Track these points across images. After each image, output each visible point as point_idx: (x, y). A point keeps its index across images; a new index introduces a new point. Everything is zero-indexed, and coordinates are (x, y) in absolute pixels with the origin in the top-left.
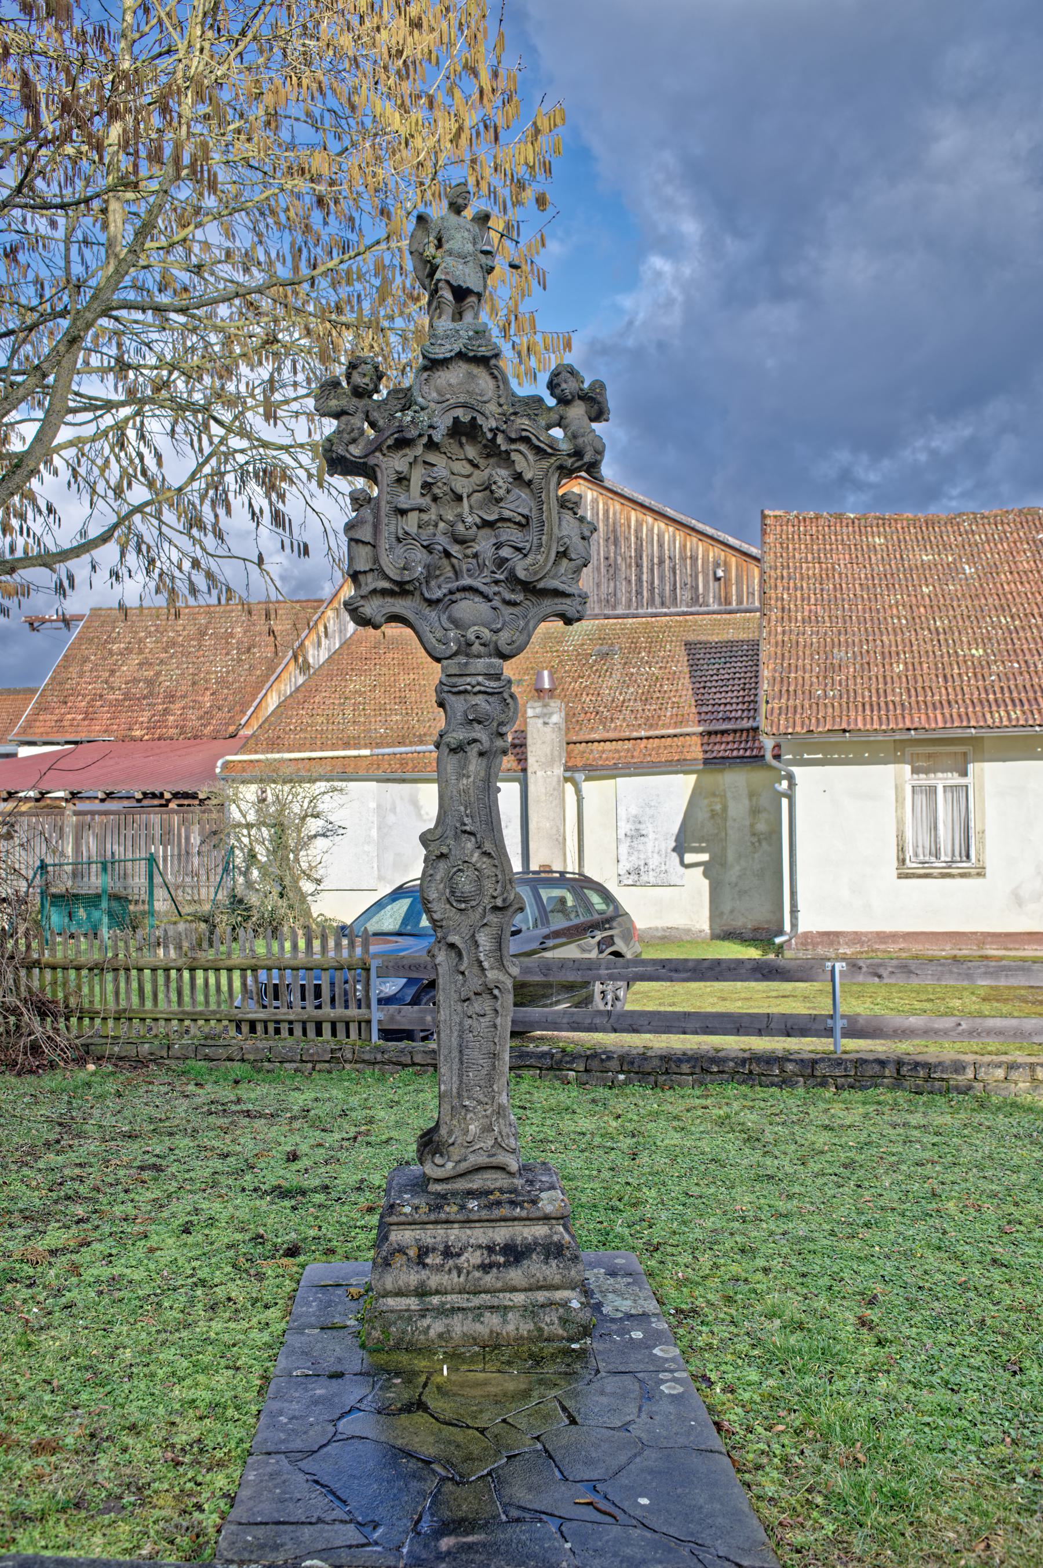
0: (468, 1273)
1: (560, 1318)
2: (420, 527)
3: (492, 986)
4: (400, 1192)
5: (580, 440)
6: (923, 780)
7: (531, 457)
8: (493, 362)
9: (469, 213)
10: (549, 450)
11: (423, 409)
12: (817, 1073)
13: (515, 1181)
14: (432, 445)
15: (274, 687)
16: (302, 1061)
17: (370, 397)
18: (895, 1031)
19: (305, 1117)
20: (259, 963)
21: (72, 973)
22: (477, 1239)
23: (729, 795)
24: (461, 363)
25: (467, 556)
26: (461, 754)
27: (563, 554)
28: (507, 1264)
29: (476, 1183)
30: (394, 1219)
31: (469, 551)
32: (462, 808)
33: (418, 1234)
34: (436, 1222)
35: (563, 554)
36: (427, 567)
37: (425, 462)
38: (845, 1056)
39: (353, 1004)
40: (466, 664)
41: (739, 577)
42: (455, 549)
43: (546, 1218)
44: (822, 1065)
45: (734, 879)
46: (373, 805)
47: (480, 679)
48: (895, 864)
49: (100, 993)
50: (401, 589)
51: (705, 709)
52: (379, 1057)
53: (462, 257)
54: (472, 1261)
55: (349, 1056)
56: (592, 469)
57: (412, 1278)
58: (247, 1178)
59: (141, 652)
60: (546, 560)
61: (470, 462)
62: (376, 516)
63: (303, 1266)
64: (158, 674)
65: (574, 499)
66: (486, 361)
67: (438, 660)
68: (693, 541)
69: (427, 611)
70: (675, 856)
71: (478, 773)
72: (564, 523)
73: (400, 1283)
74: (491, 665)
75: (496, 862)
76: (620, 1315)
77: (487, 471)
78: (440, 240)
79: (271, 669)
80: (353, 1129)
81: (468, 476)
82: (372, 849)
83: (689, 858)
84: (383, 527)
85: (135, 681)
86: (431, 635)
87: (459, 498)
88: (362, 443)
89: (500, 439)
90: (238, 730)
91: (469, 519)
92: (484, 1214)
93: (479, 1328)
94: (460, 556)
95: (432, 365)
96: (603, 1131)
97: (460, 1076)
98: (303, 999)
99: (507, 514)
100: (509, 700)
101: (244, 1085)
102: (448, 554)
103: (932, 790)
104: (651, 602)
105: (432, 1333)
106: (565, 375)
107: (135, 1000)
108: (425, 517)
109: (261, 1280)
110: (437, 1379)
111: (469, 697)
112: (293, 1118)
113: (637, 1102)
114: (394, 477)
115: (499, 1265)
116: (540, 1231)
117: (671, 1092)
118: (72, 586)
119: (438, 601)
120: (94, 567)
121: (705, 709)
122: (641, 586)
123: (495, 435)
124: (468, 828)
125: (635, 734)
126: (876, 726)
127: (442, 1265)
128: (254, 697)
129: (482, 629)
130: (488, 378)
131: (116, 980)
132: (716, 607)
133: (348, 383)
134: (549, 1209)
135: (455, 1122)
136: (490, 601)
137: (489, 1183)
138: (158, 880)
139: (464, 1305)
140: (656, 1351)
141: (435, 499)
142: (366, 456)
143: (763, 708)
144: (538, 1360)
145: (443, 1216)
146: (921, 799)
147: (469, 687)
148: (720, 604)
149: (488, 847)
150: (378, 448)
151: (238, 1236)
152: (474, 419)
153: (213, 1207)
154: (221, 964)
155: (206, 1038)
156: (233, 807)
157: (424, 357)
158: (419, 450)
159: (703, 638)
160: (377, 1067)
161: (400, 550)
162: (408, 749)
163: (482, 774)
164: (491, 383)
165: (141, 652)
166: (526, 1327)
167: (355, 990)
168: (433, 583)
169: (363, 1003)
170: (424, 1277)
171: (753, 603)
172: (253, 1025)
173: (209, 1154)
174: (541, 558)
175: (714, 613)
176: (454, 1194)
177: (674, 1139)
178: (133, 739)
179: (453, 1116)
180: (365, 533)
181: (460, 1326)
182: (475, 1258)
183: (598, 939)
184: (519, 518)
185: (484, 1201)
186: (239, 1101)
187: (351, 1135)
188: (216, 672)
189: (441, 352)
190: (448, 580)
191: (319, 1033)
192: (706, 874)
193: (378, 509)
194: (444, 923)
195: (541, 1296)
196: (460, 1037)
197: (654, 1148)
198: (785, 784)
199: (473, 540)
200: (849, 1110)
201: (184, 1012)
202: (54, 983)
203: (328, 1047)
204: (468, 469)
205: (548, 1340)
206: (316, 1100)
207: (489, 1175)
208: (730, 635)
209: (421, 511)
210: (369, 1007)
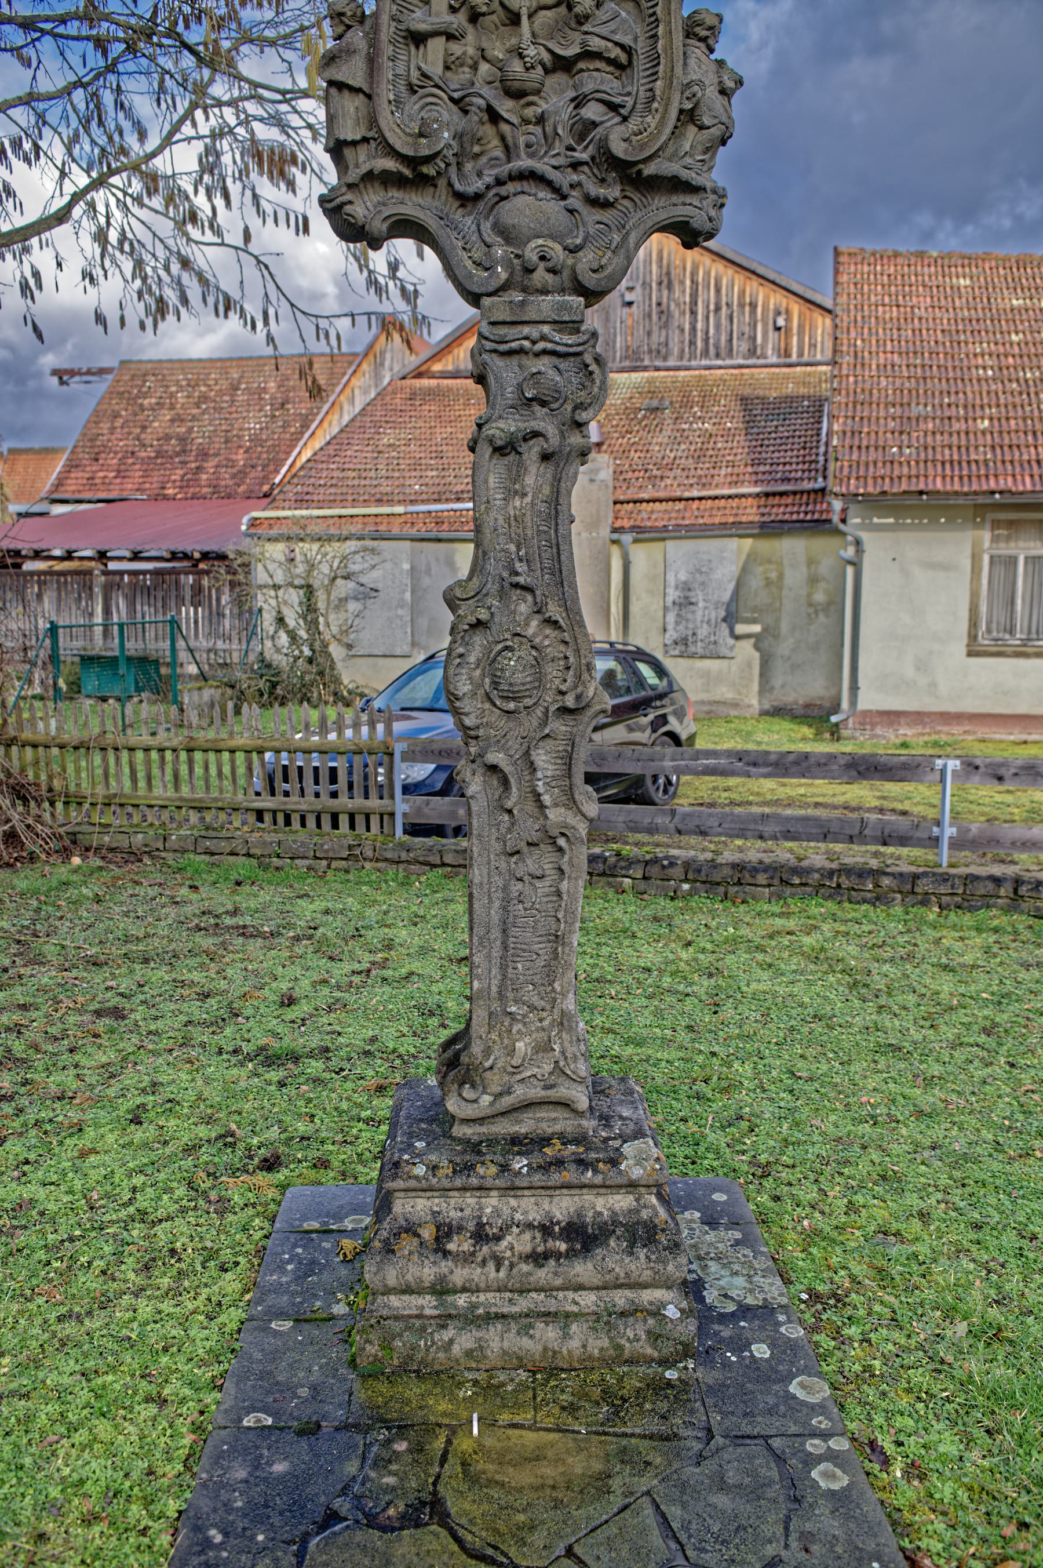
0: (512, 1266)
1: (649, 1333)
2: (447, 68)
3: (555, 832)
4: (411, 1135)
6: (1004, 550)
12: (917, 890)
13: (585, 1123)
16: (316, 858)
18: (1013, 843)
19: (310, 937)
20: (266, 745)
21: (55, 751)
22: (525, 1213)
23: (786, 562)
25: (526, 122)
26: (512, 457)
27: (689, 116)
28: (571, 1254)
29: (524, 1125)
30: (399, 1184)
31: (530, 112)
32: (512, 548)
33: (437, 1203)
34: (464, 1189)
36: (459, 136)
38: (953, 871)
39: (373, 792)
40: (523, 303)
42: (506, 107)
43: (632, 1186)
44: (924, 881)
45: (786, 652)
46: (406, 566)
47: (546, 329)
48: (965, 641)
49: (82, 775)
50: (415, 173)
51: (762, 468)
52: (404, 856)
54: (518, 1248)
55: (369, 853)
57: (428, 1272)
58: (228, 1031)
59: (172, 407)
60: (662, 123)
62: (373, 43)
63: (283, 1187)
64: (190, 430)
65: (710, 21)
68: (753, 286)
69: (458, 215)
70: (724, 629)
71: (538, 489)
72: (692, 62)
73: (409, 1277)
74: (563, 307)
75: (566, 636)
76: (731, 1308)
79: (305, 426)
80: (368, 957)
82: (404, 613)
83: (741, 629)
84: (384, 61)
85: (167, 437)
86: (465, 255)
87: (514, 19)
90: (272, 489)
91: (531, 51)
92: (537, 1178)
93: (526, 1342)
94: (515, 120)
96: (673, 967)
97: (503, 968)
98: (317, 783)
99: (596, 44)
100: (593, 367)
101: (246, 888)
102: (494, 116)
103: (1013, 561)
104: (705, 353)
105: (456, 1349)
107: (127, 783)
108: (456, 48)
109: (221, 1213)
110: (464, 1445)
111: (526, 361)
112: (297, 939)
113: (706, 919)
115: (558, 1255)
116: (622, 1202)
117: (742, 907)
118: (40, 287)
119: (478, 197)
120: (59, 265)
121: (762, 468)
124: (521, 580)
125: (687, 494)
126: (957, 487)
127: (473, 1254)
128: (289, 454)
131: (105, 760)
132: (774, 360)
134: (636, 1173)
135: (494, 1036)
136: (564, 197)
137: (544, 1125)
138: (181, 644)
139: (505, 1310)
140: (793, 1388)
141: (474, 17)
144: (617, 1403)
145: (474, 1181)
146: (1000, 571)
147: (526, 344)
149: (554, 611)
151: (203, 1132)
153: (179, 1080)
154: (222, 745)
155: (207, 829)
156: (260, 566)
159: (760, 393)
160: (402, 866)
161: (413, 105)
163: (547, 490)
165: (172, 407)
166: (599, 1344)
167: (377, 774)
168: (469, 166)
169: (385, 791)
170: (446, 1270)
172: (260, 815)
173: (185, 992)
174: (652, 121)
176: (492, 1142)
177: (762, 982)
178: (165, 497)
179: (491, 1028)
180: (353, 72)
181: (497, 1341)
182: (522, 1242)
183: (651, 717)
184: (615, 52)
185: (537, 1159)
186: (235, 912)
187: (366, 966)
190: (494, 161)
191: (335, 825)
192: (756, 647)
193: (376, 29)
194: (481, 732)
195: (621, 1298)
196: (504, 908)
197: (738, 996)
198: (850, 552)
199: (538, 92)
200: (964, 939)
201: (181, 799)
202: (36, 763)
203: (346, 842)
205: (630, 1362)
206: (327, 912)
207: (542, 1113)
208: (790, 388)
209: (450, 37)
210: (392, 797)
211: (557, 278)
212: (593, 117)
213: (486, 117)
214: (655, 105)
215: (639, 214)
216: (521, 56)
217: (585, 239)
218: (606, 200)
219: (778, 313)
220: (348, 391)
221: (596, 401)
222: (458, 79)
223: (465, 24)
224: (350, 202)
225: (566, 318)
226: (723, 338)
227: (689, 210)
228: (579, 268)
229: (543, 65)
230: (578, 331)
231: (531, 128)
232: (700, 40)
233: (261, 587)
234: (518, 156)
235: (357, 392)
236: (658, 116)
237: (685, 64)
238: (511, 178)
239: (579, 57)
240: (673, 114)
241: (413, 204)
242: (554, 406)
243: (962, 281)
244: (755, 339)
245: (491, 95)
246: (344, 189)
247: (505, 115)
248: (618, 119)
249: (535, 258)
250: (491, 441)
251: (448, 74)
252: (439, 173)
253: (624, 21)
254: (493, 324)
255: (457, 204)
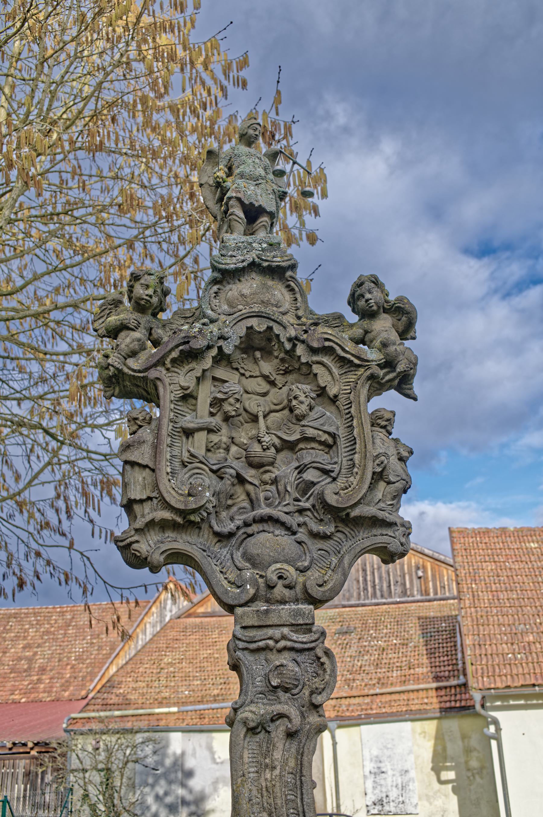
2: (208, 450)
5: (392, 349)
7: (336, 371)
8: (289, 273)
10: (356, 361)
11: (212, 321)
14: (222, 358)
15: (114, 662)
17: (154, 315)
24: (254, 275)
25: (265, 483)
26: (262, 735)
27: (379, 476)
31: (267, 477)
35: (379, 476)
37: (214, 379)
40: (267, 612)
41: (434, 576)
42: (249, 474)
47: (286, 630)
50: (187, 521)
53: (256, 179)
61: (266, 378)
64: (35, 654)
65: (387, 416)
66: (279, 272)
67: (230, 609)
69: (216, 549)
71: (285, 762)
72: (378, 441)
74: (298, 613)
77: (285, 389)
78: (230, 168)
81: (264, 395)
85: (20, 659)
87: (254, 419)
88: (143, 356)
89: (300, 350)
91: (267, 438)
94: (257, 482)
95: (224, 276)
99: (310, 432)
100: (324, 659)
102: (241, 480)
104: (374, 595)
106: (368, 285)
111: (272, 656)
114: (180, 393)
119: (231, 535)
122: (366, 584)
123: (295, 346)
125: (372, 692)
128: (100, 668)
129: (285, 566)
130: (285, 291)
132: (419, 597)
136: (294, 533)
141: (227, 418)
142: (146, 370)
143: (470, 669)
147: (271, 643)
148: (422, 595)
150: (160, 362)
152: (270, 328)
156: (74, 756)
157: (214, 268)
158: (208, 363)
161: (183, 475)
162: (205, 706)
163: (292, 763)
164: (288, 296)
168: (224, 514)
171: (445, 593)
175: (418, 601)
180: (142, 455)
184: (324, 437)
188: (75, 652)
189: (231, 264)
193: (159, 428)
199: (272, 464)
204: (264, 387)
209: (210, 431)
211: (292, 592)
212: (312, 479)
213: (236, 481)
214: (356, 470)
215: (350, 543)
216: (259, 442)
217: (311, 562)
218: (324, 533)
219: (418, 568)
220: (142, 626)
221: (329, 686)
222: (214, 458)
223: (220, 422)
224: (137, 542)
225: (301, 622)
226: (385, 585)
227: (385, 539)
228: (308, 584)
229: (274, 445)
230: (310, 631)
231: (268, 487)
232: (382, 427)
233: (73, 771)
234: (259, 506)
235: (148, 626)
236: (358, 477)
237: (373, 443)
238: (255, 521)
239: (299, 441)
240: (369, 475)
241: (182, 542)
242: (295, 691)
243: (532, 545)
244: (404, 584)
245: (240, 466)
246: (133, 532)
247: (250, 479)
248: (329, 480)
249: (275, 578)
250: (245, 722)
251: (209, 454)
252: (202, 520)
253: (329, 418)
254: (244, 628)
255: (216, 540)
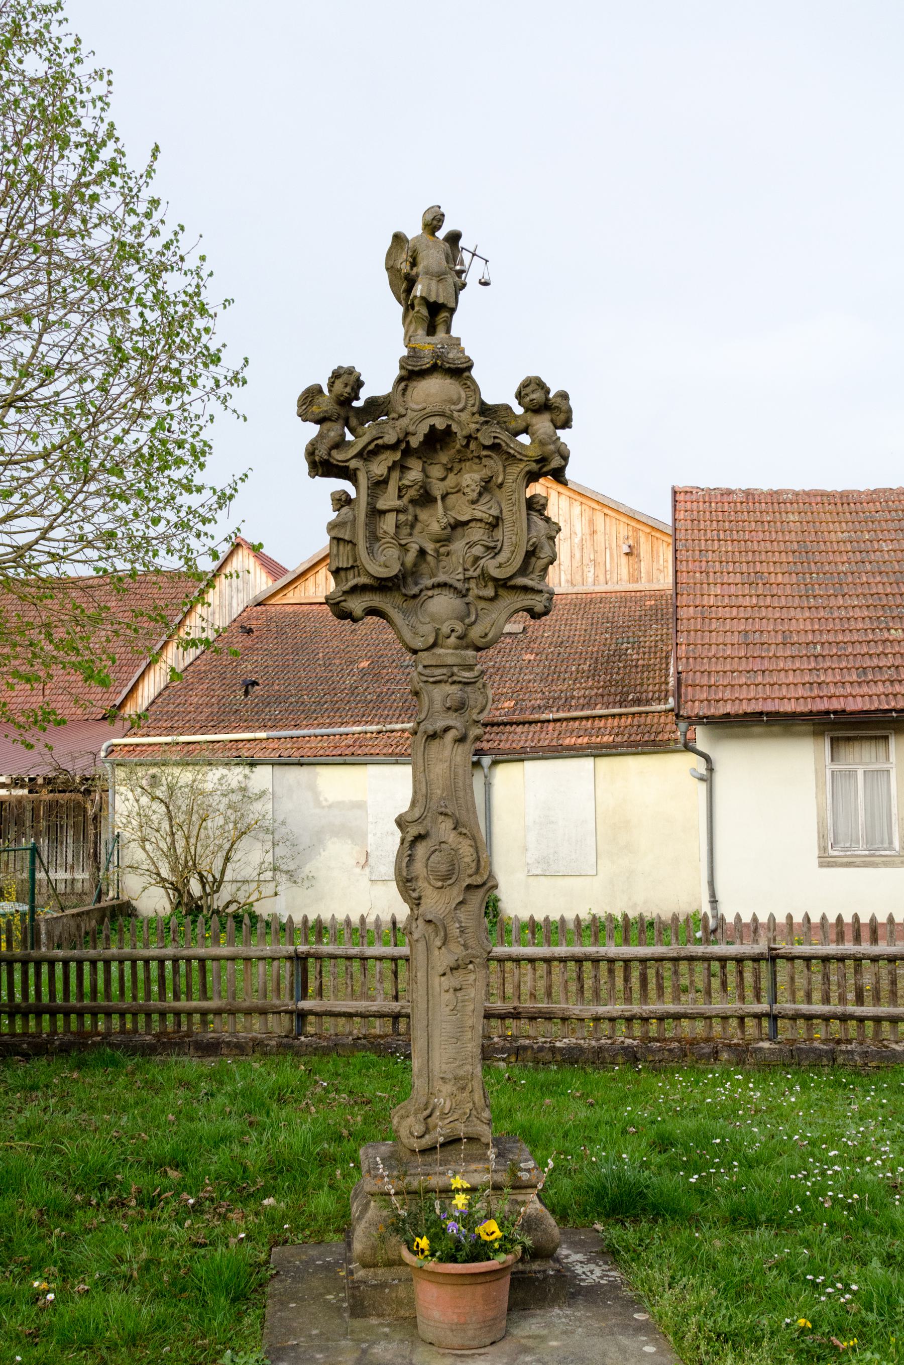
9: (441, 234)
10: (519, 456)
56: (558, 475)
133: (330, 391)
152: (449, 426)
241: (375, 600)
